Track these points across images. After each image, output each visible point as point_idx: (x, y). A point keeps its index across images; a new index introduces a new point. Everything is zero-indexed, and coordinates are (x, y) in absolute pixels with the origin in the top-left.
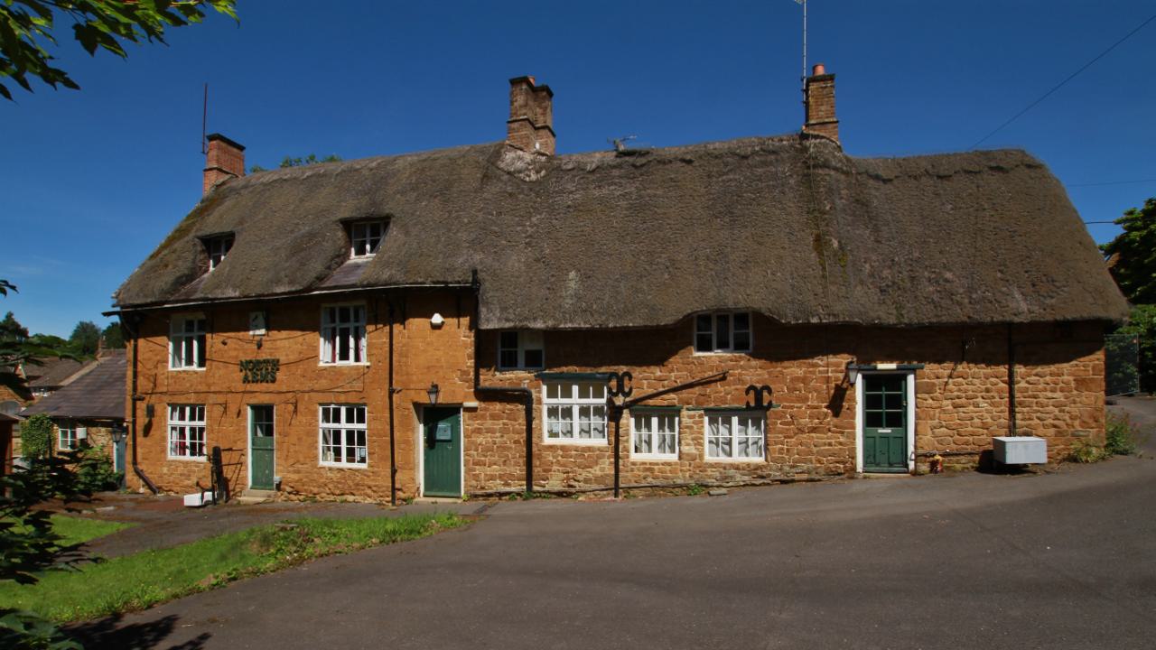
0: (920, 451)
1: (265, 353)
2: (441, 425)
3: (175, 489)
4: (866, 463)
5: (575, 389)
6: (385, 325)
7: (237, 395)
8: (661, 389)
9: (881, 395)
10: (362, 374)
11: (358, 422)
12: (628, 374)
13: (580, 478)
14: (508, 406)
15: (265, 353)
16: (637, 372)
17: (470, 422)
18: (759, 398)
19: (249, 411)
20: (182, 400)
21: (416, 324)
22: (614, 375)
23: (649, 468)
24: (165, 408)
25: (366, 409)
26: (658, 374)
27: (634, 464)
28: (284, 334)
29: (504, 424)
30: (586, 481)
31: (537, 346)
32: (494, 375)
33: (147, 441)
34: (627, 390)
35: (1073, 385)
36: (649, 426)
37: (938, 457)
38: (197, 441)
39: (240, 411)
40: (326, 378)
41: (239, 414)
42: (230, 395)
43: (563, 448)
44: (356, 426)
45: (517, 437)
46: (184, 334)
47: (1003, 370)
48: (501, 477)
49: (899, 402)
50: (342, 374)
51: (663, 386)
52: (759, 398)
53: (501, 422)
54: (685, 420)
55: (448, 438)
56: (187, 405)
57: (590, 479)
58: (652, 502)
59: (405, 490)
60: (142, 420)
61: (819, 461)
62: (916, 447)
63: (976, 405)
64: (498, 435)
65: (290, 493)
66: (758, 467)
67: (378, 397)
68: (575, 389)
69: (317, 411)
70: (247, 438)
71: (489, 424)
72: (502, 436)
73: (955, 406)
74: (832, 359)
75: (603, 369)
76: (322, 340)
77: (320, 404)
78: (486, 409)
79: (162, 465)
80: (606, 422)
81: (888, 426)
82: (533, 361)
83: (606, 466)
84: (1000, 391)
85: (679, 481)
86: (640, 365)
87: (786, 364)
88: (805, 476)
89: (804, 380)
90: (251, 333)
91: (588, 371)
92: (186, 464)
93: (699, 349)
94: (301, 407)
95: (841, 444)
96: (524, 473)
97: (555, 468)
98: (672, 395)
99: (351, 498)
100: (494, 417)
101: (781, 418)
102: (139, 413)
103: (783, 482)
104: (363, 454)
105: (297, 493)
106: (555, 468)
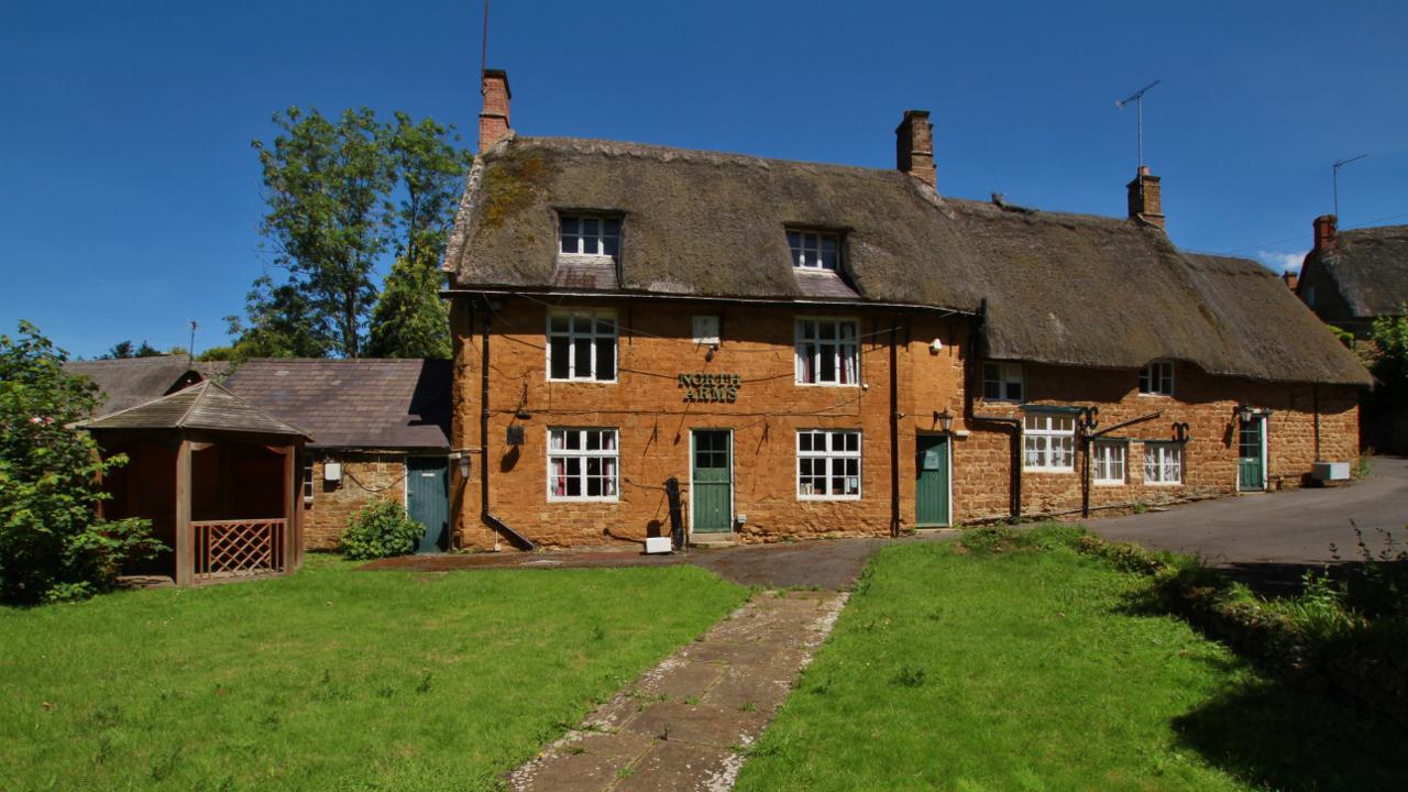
0: (1271, 474)
1: (719, 366)
2: (930, 454)
3: (563, 541)
4: (696, 526)
5: (1049, 421)
6: (884, 346)
7: (674, 416)
8: (1118, 424)
9: (708, 455)
10: (856, 397)
11: (848, 449)
12: (1095, 409)
13: (1054, 502)
14: (995, 436)
15: (719, 366)
16: (1102, 408)
17: (960, 451)
18: (1180, 434)
19: (691, 438)
20: (577, 421)
21: (919, 347)
22: (1085, 409)
23: (1108, 491)
24: (545, 432)
25: (860, 435)
26: (1116, 410)
27: (1097, 488)
28: (746, 345)
29: (991, 453)
30: (1060, 505)
31: (1016, 379)
32: (982, 405)
33: (510, 478)
34: (1094, 423)
35: (1344, 429)
36: (1103, 456)
37: (1282, 478)
38: (601, 476)
39: (679, 437)
40: (807, 400)
41: (677, 440)
42: (662, 417)
43: (1040, 475)
44: (845, 454)
45: (1002, 465)
46: (817, 342)
47: (1311, 416)
48: (988, 505)
49: (1257, 438)
50: (831, 396)
51: (1119, 421)
52: (1180, 434)
53: (988, 451)
54: (1133, 451)
55: (936, 467)
56: (583, 428)
57: (1063, 504)
58: (1112, 521)
59: (906, 520)
60: (498, 447)
61: (1217, 483)
62: (1268, 471)
63: (1299, 441)
64: (986, 463)
65: (754, 534)
66: (1180, 489)
67: (880, 421)
68: (1049, 421)
69: (794, 437)
70: (688, 470)
71: (977, 452)
72: (989, 465)
73: (1289, 442)
74: (1225, 404)
75: (1076, 404)
76: (796, 356)
77: (799, 429)
78: (974, 438)
79: (538, 511)
80: (1072, 452)
81: (1251, 456)
82: (1013, 393)
83: (1075, 492)
84: (1310, 432)
85: (1129, 502)
86: (1103, 401)
87: (1197, 406)
88: (1208, 495)
89: (1208, 419)
90: (696, 341)
91: (1064, 404)
92: (584, 507)
93: (1141, 391)
94: (773, 433)
95: (1229, 469)
96: (1008, 499)
97: (1034, 494)
98: (1124, 429)
99: (839, 534)
100: (981, 446)
101: (1194, 449)
102: (491, 438)
103: (1194, 500)
104: (854, 485)
105: (765, 533)
106: (1034, 494)
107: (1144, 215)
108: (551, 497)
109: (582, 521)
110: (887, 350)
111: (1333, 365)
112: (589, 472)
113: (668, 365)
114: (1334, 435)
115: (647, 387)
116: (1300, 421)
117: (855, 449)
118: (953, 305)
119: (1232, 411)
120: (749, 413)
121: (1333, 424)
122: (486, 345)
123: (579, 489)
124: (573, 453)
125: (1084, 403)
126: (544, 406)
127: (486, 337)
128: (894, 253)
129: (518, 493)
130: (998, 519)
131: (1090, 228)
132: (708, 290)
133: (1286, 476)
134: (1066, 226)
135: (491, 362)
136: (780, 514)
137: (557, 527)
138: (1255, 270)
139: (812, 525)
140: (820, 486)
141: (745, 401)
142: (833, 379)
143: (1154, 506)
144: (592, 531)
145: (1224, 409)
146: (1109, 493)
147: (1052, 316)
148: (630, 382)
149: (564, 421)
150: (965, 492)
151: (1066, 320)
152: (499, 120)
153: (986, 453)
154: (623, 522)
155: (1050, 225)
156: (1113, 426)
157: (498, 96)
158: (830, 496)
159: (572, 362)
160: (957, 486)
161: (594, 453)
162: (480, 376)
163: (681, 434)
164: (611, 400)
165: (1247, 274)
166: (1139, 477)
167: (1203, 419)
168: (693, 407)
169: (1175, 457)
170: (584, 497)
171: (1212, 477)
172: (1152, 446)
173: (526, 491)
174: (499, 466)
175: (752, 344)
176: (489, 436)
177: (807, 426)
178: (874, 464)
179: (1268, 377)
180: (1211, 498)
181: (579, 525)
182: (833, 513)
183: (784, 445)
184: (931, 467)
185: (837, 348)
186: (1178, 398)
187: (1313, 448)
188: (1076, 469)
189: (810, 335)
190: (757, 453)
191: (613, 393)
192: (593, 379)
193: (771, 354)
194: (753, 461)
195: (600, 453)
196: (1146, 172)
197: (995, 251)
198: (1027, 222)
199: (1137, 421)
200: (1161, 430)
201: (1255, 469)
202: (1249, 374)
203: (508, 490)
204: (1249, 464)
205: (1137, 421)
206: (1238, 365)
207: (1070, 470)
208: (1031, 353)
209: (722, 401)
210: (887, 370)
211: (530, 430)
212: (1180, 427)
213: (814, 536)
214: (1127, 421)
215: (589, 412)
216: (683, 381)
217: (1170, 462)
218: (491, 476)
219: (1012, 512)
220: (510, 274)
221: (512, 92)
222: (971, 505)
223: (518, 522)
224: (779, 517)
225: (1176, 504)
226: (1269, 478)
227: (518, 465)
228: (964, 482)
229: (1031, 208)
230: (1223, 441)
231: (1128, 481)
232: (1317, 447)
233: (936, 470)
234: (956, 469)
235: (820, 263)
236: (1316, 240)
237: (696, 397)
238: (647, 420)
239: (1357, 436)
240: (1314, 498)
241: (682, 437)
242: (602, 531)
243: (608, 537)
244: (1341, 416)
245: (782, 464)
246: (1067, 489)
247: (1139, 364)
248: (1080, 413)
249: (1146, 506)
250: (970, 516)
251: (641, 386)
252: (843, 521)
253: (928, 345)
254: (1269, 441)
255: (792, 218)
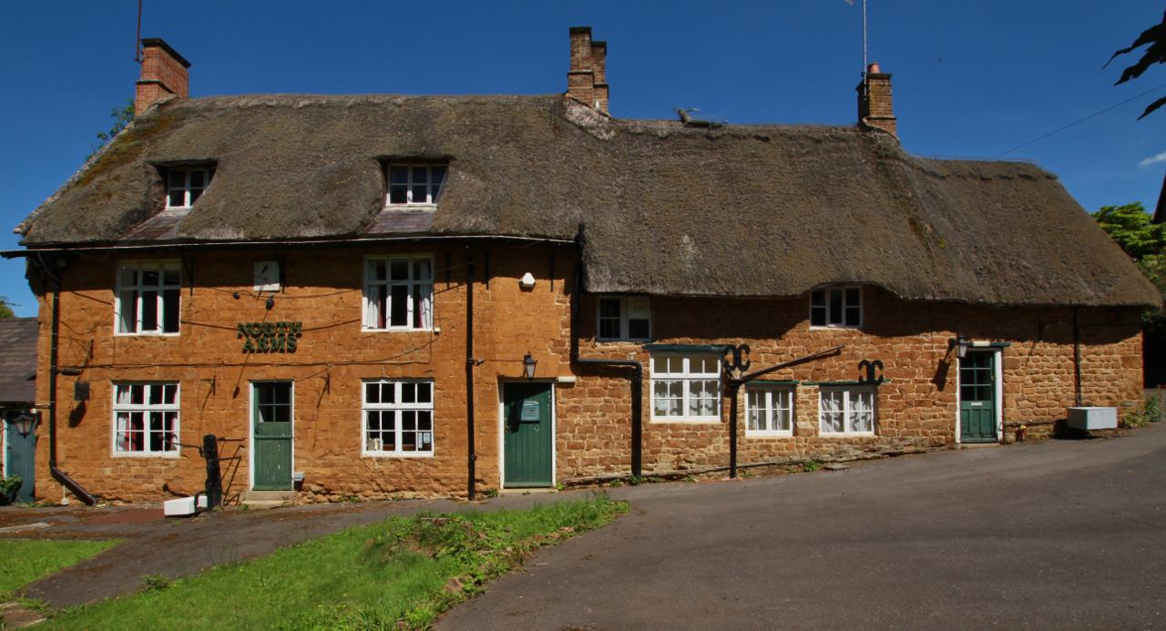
0: (1008, 422)
2: (528, 404)
3: (125, 496)
5: (686, 362)
6: (460, 284)
7: (232, 368)
8: (779, 364)
14: (611, 381)
16: (755, 345)
18: (871, 373)
20: (139, 375)
21: (502, 284)
22: (732, 347)
23: (766, 445)
24: (109, 387)
25: (432, 384)
26: (776, 347)
28: (309, 290)
29: (606, 401)
30: (699, 462)
33: (77, 433)
34: (744, 363)
35: (1120, 362)
36: (762, 404)
38: (164, 431)
39: (238, 389)
42: (221, 369)
43: (673, 427)
44: (417, 406)
45: (621, 415)
46: (389, 282)
47: (1069, 348)
48: (601, 461)
49: (987, 377)
50: (400, 342)
51: (781, 360)
52: (871, 373)
53: (602, 399)
54: (801, 395)
56: (147, 382)
57: (704, 460)
60: (67, 403)
61: (925, 434)
62: (1004, 418)
63: (1050, 380)
64: (599, 413)
66: (870, 441)
67: (454, 369)
68: (686, 362)
69: (359, 388)
71: (588, 401)
73: (1035, 381)
74: (936, 336)
75: (720, 341)
76: (365, 300)
77: (364, 380)
78: (584, 385)
80: (719, 398)
82: (638, 331)
83: (721, 445)
85: (796, 458)
86: (757, 337)
87: (895, 339)
88: (912, 449)
89: (911, 355)
90: (256, 288)
91: (703, 343)
93: (814, 323)
94: (335, 383)
95: (944, 416)
97: (664, 448)
98: (789, 370)
99: (409, 494)
100: (593, 394)
102: (60, 394)
103: (891, 455)
104: (427, 440)
105: (328, 492)
106: (664, 448)
107: (869, 119)
108: (117, 452)
109: (142, 476)
110: (464, 288)
111: (1099, 282)
112: (153, 427)
113: (228, 314)
114: (1104, 370)
115: (206, 339)
116: (1051, 355)
117: (428, 400)
118: (540, 232)
119: (946, 344)
120: (310, 363)
121: (1103, 356)
122: (57, 303)
123: (142, 444)
124: (137, 407)
125: (729, 341)
126: (109, 361)
127: (57, 295)
128: (483, 179)
129: (84, 447)
130: (615, 478)
131: (790, 138)
132: (256, 235)
133: (1028, 425)
134: (757, 138)
135: (62, 318)
136: (344, 471)
137: (120, 482)
138: (1022, 173)
139: (378, 485)
140: (389, 442)
141: (306, 350)
142: (404, 323)
143: (832, 462)
144: (151, 487)
145: (936, 342)
146: (768, 447)
147: (686, 239)
148: (190, 334)
149: (128, 375)
150: (572, 447)
151: (702, 242)
152: (153, 86)
153: (600, 402)
154: (182, 478)
155: (739, 138)
156: (772, 366)
157: (154, 63)
158: (399, 452)
159: (140, 316)
160: (562, 441)
161: (157, 407)
162: (50, 332)
163: (240, 386)
164: (171, 353)
165: (1021, 176)
166: (810, 427)
167: (903, 355)
168: (252, 358)
169: (866, 401)
170: (147, 452)
171: (918, 426)
172: (831, 390)
173: (92, 446)
174: (67, 420)
175: (315, 288)
176: (58, 392)
177: (372, 376)
178: (447, 416)
179: (994, 301)
180: (917, 452)
181: (140, 480)
182: (401, 470)
183: (347, 396)
184: (528, 419)
185: (411, 289)
186: (867, 330)
187: (1073, 388)
188: (723, 419)
189: (382, 276)
190: (318, 406)
191: (174, 346)
192: (159, 332)
193: (335, 298)
194: (313, 415)
195: (163, 407)
196: (876, 69)
197: (651, 171)
198: (708, 137)
199: (807, 360)
200: (843, 369)
201: (985, 418)
202: (964, 298)
203: (75, 445)
204: (977, 409)
205: (807, 360)
206: (947, 286)
207: (716, 420)
208: (644, 283)
209: (282, 351)
210: (464, 312)
211: (96, 387)
212: (870, 367)
213: (382, 495)
214: (792, 359)
215: (150, 366)
216: (243, 331)
217: (861, 408)
218: (60, 431)
219: (633, 470)
220: (69, 232)
221: (185, 56)
222: (580, 461)
223: (83, 476)
224: (341, 475)
225: (866, 459)
226: (1005, 426)
227: (85, 420)
228: (571, 435)
229: (717, 122)
230: (932, 382)
231: (796, 433)
232: (1078, 386)
233: (537, 422)
234: (560, 420)
235: (429, 197)
236: (184, 60)
237: (255, 347)
238: (206, 373)
239: (1141, 371)
240: (1068, 455)
241: (241, 390)
242: (161, 486)
243: (167, 493)
244: (1115, 346)
245: (345, 417)
246: (710, 442)
247: (796, 290)
248: (725, 353)
249: (822, 462)
250: (579, 475)
251: (202, 338)
252: (413, 481)
253: (518, 280)
254: (1004, 380)
255: (387, 152)
